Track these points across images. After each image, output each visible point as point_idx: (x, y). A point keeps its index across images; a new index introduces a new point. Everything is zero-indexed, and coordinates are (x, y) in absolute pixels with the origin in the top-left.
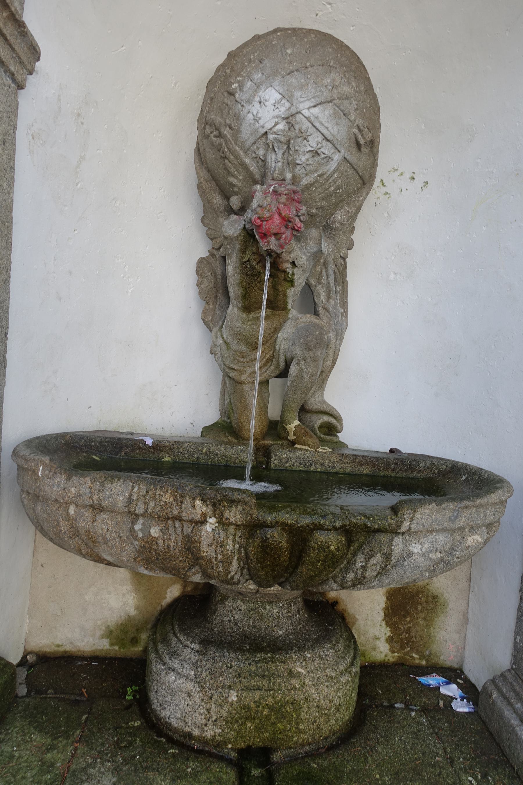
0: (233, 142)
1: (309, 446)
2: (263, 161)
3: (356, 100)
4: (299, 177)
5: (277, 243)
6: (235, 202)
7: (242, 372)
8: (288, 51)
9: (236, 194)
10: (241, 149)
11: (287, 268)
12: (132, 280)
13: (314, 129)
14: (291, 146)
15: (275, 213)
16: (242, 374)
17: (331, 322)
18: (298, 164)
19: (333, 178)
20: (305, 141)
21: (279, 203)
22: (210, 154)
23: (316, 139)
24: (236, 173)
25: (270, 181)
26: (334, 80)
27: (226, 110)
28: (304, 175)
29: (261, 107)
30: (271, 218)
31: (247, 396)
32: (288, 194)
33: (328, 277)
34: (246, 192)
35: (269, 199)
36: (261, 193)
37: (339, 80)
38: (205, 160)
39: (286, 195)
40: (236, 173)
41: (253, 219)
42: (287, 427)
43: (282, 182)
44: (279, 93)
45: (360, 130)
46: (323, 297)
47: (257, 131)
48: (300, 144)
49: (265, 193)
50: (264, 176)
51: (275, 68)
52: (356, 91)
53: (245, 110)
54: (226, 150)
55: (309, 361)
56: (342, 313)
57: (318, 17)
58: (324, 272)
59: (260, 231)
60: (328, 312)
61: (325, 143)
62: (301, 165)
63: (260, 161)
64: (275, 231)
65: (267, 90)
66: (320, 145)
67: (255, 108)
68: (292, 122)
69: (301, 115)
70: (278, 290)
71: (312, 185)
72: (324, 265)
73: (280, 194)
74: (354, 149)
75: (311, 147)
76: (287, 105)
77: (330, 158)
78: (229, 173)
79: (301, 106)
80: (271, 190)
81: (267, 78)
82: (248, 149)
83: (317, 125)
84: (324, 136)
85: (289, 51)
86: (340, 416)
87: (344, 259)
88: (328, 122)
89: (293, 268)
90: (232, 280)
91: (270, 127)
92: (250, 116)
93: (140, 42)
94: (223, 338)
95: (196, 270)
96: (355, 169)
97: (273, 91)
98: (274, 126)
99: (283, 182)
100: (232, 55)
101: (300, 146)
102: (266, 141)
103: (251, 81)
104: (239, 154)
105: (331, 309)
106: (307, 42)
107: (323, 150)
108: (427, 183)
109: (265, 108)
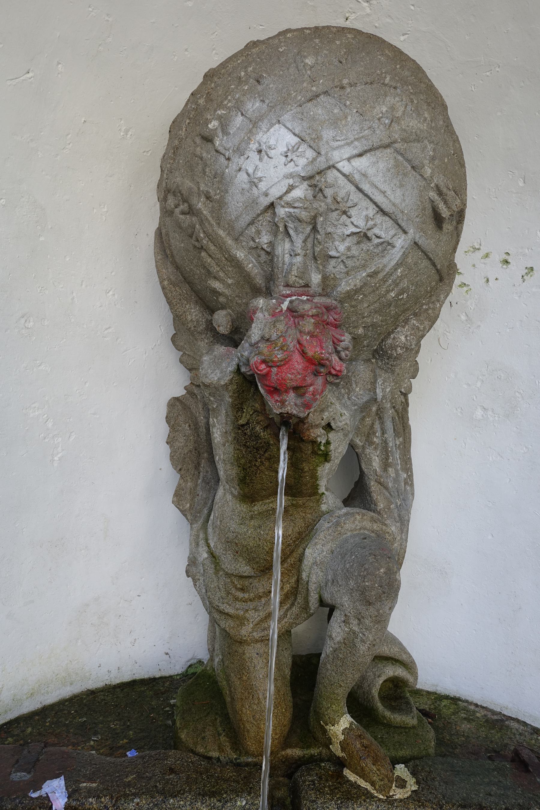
0: (213, 222)
1: (373, 784)
2: (268, 253)
3: (433, 142)
4: (335, 279)
5: (299, 401)
6: (222, 320)
7: (241, 621)
8: (307, 61)
9: (223, 308)
10: (229, 234)
11: (318, 436)
12: (60, 439)
13: (361, 195)
14: (319, 226)
15: (293, 352)
16: (242, 624)
17: (392, 506)
18: (331, 257)
19: (394, 277)
20: (344, 217)
21: (301, 332)
22: (178, 242)
23: (364, 213)
24: (221, 274)
25: (281, 288)
26: (392, 108)
27: (200, 167)
28: (343, 275)
29: (261, 159)
30: (286, 361)
31: (252, 669)
32: (317, 315)
33: (383, 432)
34: (239, 305)
35: (281, 327)
36: (266, 314)
37: (403, 109)
38: (170, 250)
39: (312, 316)
40: (221, 274)
41: (252, 362)
42: (327, 727)
43: (304, 289)
44: (295, 134)
45: (440, 193)
46: (376, 463)
47: (255, 202)
48: (335, 223)
49: (275, 314)
50: (270, 278)
51: (284, 90)
52: (432, 128)
53: (233, 166)
54: (202, 235)
55: (367, 622)
56: (405, 479)
57: (348, 22)
58: (377, 426)
59: (267, 383)
60: (386, 488)
61: (379, 218)
62: (338, 258)
63: (263, 253)
64: (295, 384)
65: (272, 130)
66: (371, 223)
67: (251, 163)
68: (320, 185)
69: (335, 171)
70: (302, 470)
71: (357, 291)
72: (377, 414)
73: (302, 316)
74: (431, 226)
75: (356, 226)
76: (310, 154)
77: (389, 244)
78: (209, 274)
79: (336, 155)
80: (285, 306)
81: (271, 108)
82: (241, 234)
83: (366, 187)
84: (377, 206)
85: (309, 61)
86: (413, 662)
87: (405, 395)
88: (385, 181)
89: (328, 432)
90: (221, 452)
91: (278, 194)
92: (242, 177)
93: (60, 66)
94: (208, 546)
95: (167, 417)
96: (430, 259)
97: (283, 131)
98: (287, 192)
99: (306, 289)
100: (209, 76)
101: (335, 226)
102: (273, 218)
103: (242, 114)
104: (224, 243)
105: (390, 485)
106: (341, 44)
107: (376, 231)
108: (532, 269)
109: (271, 161)
